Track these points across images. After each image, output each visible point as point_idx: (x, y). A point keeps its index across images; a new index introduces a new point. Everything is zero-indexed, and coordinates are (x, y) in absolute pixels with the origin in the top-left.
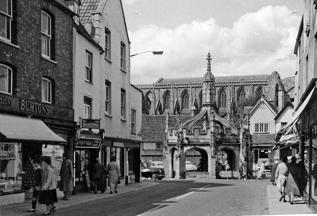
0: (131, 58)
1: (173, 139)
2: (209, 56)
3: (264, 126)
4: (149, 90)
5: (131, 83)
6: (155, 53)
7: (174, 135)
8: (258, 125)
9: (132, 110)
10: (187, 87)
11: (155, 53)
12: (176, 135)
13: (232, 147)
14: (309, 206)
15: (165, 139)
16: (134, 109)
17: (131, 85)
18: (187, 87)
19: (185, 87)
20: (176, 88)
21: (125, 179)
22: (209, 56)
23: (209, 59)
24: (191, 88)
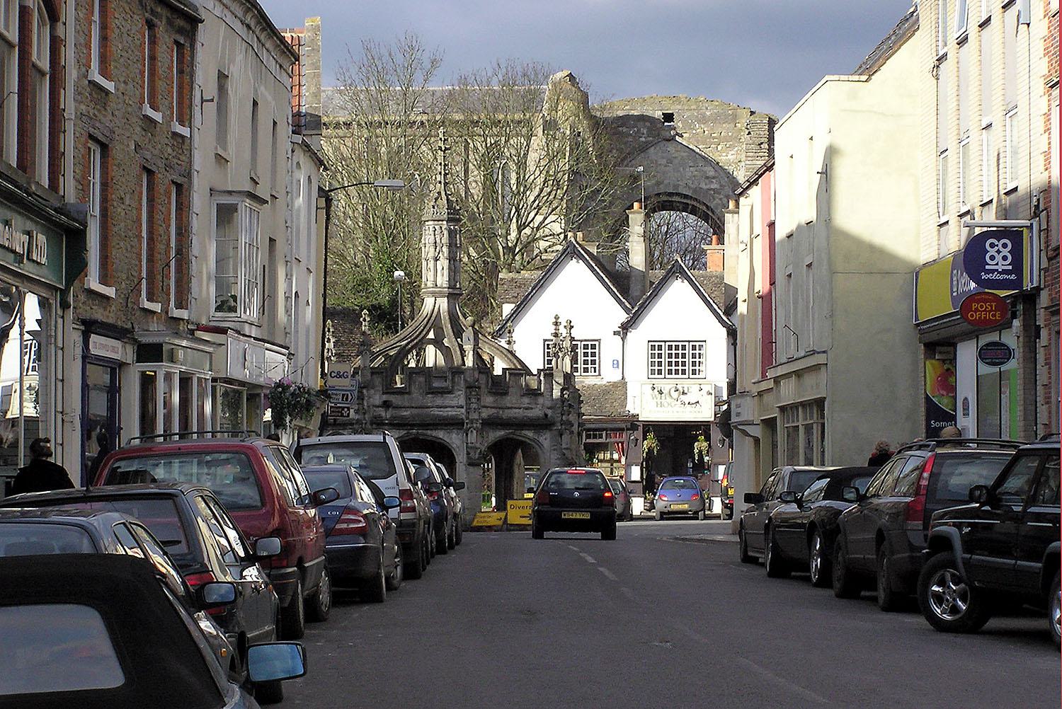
8: (660, 348)
13: (530, 434)
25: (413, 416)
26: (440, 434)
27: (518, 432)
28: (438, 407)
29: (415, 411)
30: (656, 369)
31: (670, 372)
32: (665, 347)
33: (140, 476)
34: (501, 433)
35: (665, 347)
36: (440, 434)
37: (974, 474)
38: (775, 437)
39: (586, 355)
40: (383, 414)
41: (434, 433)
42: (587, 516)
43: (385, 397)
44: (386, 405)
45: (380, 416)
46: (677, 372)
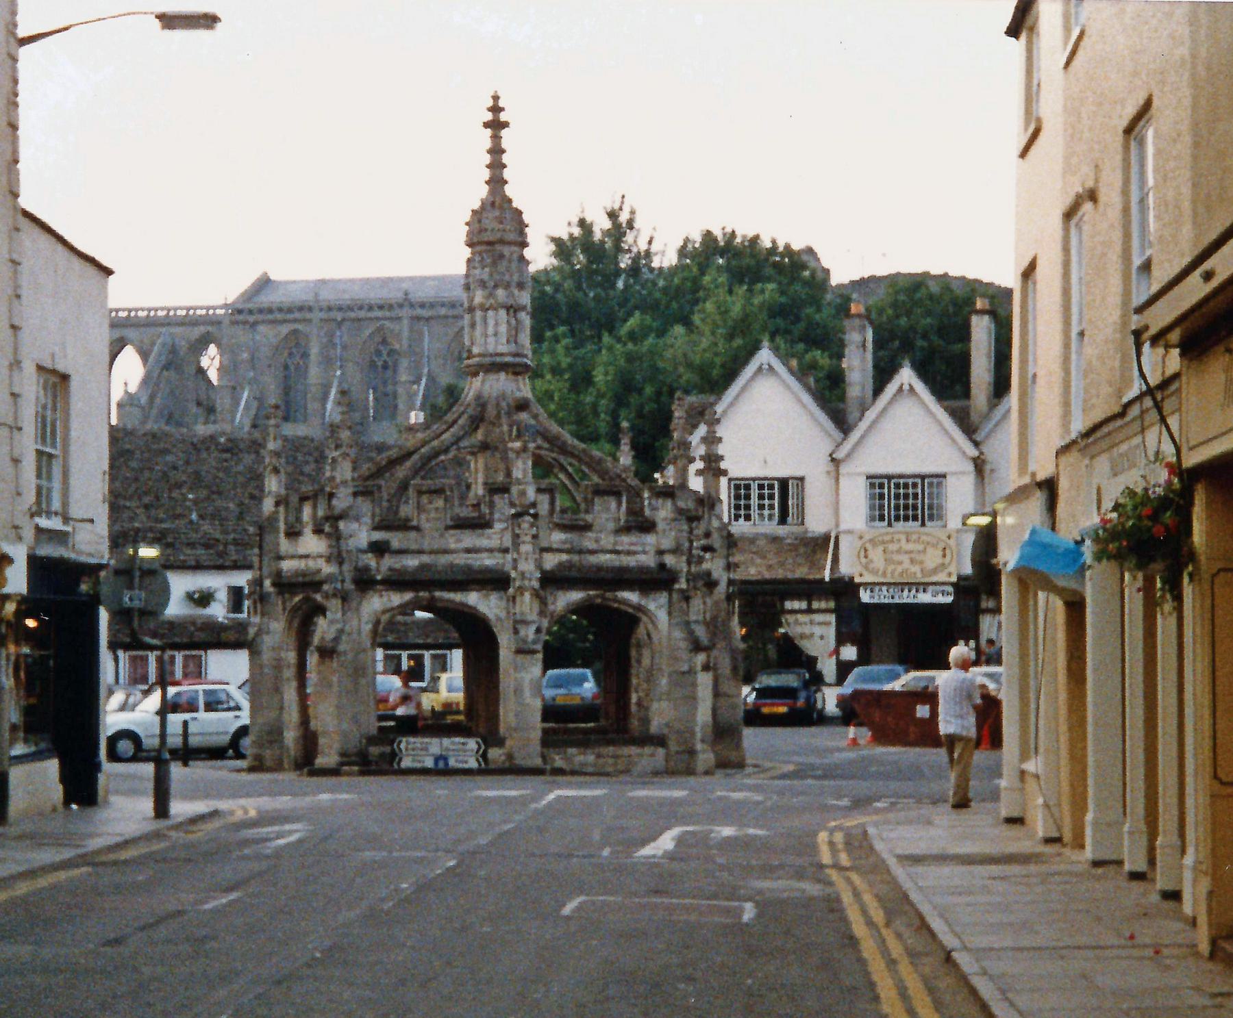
0: (24, 52)
1: (301, 551)
2: (496, 109)
3: (754, 493)
4: (202, 329)
5: (25, 202)
6: (169, 21)
7: (308, 531)
8: (748, 487)
9: (40, 368)
10: (390, 319)
11: (169, 21)
12: (318, 531)
13: (632, 597)
14: (351, 536)
15: (261, 556)
16: (61, 367)
17: (27, 214)
18: (390, 319)
19: (378, 319)
20: (335, 320)
21: (316, 640)
22: (496, 109)
23: (496, 125)
24: (405, 322)
25: (423, 567)
26: (473, 598)
27: (609, 595)
28: (468, 551)
29: (426, 559)
30: (878, 514)
31: (897, 518)
32: (754, 486)
33: (256, 612)
34: (576, 596)
35: (754, 486)
36: (473, 598)
37: (1080, 911)
38: (272, 836)
39: (761, 497)
40: (373, 564)
41: (457, 597)
42: (783, 709)
43: (378, 536)
44: (379, 549)
45: (367, 569)
46: (906, 519)
